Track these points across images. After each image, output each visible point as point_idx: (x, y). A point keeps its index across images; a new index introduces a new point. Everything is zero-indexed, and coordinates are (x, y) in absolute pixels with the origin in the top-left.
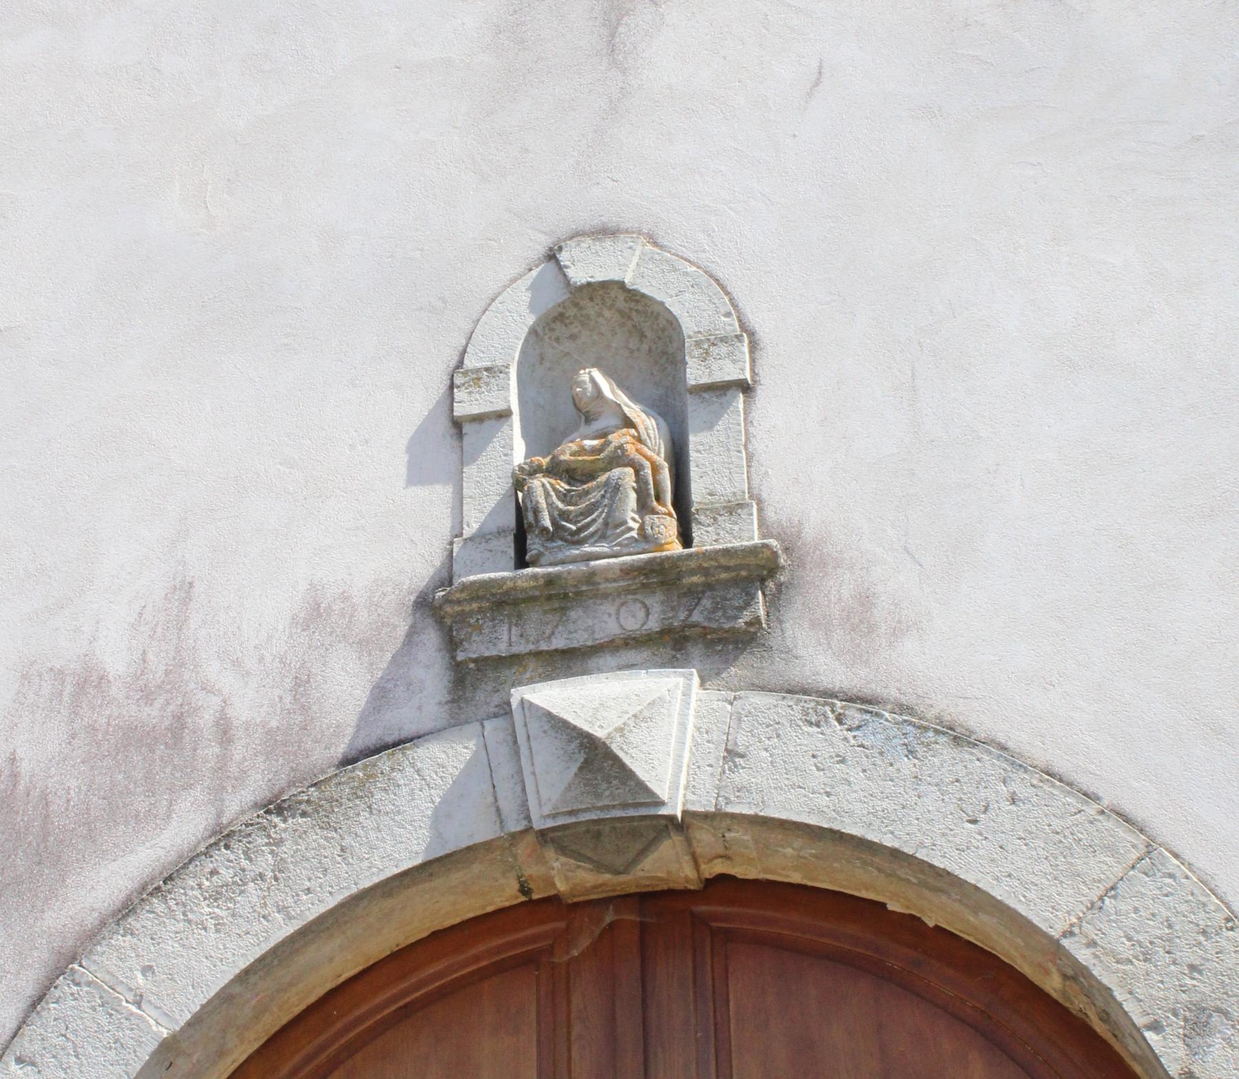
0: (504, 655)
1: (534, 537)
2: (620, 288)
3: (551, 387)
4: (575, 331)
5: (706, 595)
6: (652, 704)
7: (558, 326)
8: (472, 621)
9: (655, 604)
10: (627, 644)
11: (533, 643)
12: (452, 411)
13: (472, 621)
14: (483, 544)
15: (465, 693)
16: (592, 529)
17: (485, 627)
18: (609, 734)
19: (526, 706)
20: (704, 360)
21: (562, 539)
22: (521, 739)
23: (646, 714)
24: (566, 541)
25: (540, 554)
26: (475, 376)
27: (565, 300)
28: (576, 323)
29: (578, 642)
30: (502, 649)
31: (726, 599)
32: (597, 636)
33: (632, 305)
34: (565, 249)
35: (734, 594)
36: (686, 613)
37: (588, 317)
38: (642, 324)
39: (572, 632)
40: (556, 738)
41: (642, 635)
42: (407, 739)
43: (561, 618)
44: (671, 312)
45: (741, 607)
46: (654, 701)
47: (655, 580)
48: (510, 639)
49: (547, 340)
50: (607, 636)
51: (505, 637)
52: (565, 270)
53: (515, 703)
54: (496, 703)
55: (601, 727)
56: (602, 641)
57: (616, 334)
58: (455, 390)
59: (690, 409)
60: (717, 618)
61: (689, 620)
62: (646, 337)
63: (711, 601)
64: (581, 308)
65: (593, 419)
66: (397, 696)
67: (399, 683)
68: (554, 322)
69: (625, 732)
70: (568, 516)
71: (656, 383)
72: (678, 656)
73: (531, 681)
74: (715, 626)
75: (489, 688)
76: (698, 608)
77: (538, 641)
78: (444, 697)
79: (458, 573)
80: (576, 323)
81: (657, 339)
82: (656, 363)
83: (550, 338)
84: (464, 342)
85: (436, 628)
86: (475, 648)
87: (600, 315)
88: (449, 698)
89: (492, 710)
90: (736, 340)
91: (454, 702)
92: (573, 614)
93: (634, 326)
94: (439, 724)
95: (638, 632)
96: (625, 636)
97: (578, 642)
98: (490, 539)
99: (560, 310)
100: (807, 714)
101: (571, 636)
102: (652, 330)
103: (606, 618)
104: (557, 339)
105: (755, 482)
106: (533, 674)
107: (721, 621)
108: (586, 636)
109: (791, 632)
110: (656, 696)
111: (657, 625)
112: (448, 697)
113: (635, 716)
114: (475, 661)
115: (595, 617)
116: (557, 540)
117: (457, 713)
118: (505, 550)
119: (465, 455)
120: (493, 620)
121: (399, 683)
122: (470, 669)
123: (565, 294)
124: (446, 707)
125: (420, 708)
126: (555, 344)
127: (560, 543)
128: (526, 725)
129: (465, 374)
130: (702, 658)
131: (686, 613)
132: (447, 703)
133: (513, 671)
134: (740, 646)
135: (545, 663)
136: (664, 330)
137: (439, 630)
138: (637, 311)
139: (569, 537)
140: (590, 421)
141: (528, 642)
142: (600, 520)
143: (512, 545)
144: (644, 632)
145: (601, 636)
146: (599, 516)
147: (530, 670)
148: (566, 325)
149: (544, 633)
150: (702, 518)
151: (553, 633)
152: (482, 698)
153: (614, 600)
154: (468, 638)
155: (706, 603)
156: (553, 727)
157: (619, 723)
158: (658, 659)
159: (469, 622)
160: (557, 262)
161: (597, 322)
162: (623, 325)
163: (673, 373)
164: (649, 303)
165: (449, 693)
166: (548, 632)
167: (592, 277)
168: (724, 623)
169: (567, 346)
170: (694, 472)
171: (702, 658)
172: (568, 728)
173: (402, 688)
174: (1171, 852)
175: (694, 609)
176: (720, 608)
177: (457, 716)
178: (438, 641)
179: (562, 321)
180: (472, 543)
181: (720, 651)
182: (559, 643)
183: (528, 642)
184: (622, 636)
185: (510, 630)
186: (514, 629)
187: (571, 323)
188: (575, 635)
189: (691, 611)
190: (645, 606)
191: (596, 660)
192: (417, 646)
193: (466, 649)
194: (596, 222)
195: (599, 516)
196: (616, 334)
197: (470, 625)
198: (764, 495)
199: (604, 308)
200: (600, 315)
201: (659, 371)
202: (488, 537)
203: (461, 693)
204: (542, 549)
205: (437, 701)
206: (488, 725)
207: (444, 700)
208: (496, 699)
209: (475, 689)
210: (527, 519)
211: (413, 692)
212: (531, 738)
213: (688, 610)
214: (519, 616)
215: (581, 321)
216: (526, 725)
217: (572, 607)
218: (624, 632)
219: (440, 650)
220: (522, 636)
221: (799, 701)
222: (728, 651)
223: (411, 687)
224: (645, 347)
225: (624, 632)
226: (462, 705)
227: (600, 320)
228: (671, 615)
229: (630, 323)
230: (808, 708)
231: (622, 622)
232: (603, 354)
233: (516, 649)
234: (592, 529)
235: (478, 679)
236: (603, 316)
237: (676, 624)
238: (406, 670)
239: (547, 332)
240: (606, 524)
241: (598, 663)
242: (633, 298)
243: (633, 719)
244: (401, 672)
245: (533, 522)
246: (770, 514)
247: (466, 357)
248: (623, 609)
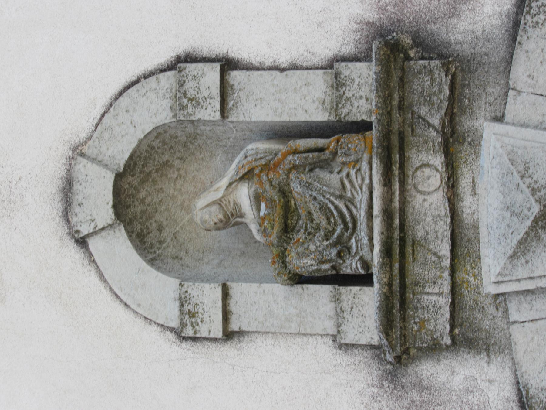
0: (450, 300)
1: (344, 265)
2: (121, 178)
3: (203, 253)
4: (154, 225)
5: (417, 110)
6: (512, 163)
7: (148, 240)
8: (415, 328)
9: (419, 159)
10: (453, 186)
11: (443, 272)
12: (215, 340)
13: (415, 328)
14: (345, 314)
15: (482, 339)
16: (345, 210)
17: (423, 316)
18: (536, 201)
19: (500, 279)
20: (198, 103)
21: (350, 239)
22: (530, 285)
23: (521, 168)
24: (352, 234)
25: (362, 259)
26: (187, 316)
27: (126, 230)
28: (148, 224)
29: (446, 230)
30: (444, 302)
31: (422, 92)
32: (443, 213)
33: (138, 170)
34: (79, 228)
35: (419, 84)
36: (431, 129)
37: (143, 212)
38: (156, 163)
39: (437, 236)
40: (534, 252)
41: (447, 171)
42: (518, 394)
43: (422, 246)
44: (150, 132)
45: (431, 78)
46: (510, 160)
47: (398, 156)
48: (436, 294)
49: (160, 251)
50: (444, 204)
51: (434, 298)
52: (97, 229)
53: (494, 290)
54: (495, 309)
55: (529, 209)
56: (448, 208)
57: (161, 189)
58: (198, 335)
59: (241, 118)
60: (439, 101)
61: (437, 127)
62: (168, 161)
63: (422, 107)
64: (135, 217)
65: (240, 211)
66: (476, 403)
67: (465, 400)
68: (144, 243)
69: (536, 187)
70: (329, 231)
71: (210, 156)
72: (469, 140)
73: (478, 276)
74: (446, 104)
75: (480, 316)
76: (427, 119)
77: (441, 268)
78: (483, 358)
79: (369, 340)
80: (148, 224)
81: (172, 151)
82: (193, 154)
83: (159, 249)
84: (154, 327)
85: (418, 363)
86: (441, 327)
87: (143, 201)
88: (485, 353)
89: (500, 313)
90: (183, 73)
91: (489, 350)
92: (420, 234)
93: (157, 171)
94: (508, 363)
95: (444, 175)
96: (446, 187)
97: (446, 230)
98: (341, 309)
99: (134, 236)
100: (537, 23)
101: (440, 237)
102: (163, 154)
103: (426, 204)
104: (161, 242)
105: (317, 61)
106: (471, 274)
107: (442, 98)
108: (442, 223)
109: (459, 35)
110: (506, 158)
111: (439, 157)
112: (484, 355)
113: (522, 177)
114: (453, 327)
115: (425, 214)
116: (350, 244)
117: (500, 347)
118: (353, 296)
119: (259, 330)
120: (417, 308)
121: (465, 400)
122: (459, 332)
123: (120, 230)
124: (492, 356)
125: (491, 382)
126: (165, 245)
127: (353, 240)
128: (519, 280)
129: (183, 325)
130: (475, 118)
131: (431, 129)
132: (488, 356)
133: (466, 293)
134: (467, 82)
135: (462, 263)
136: (164, 143)
137: (420, 360)
138: (143, 166)
139: (349, 232)
140: (242, 213)
141: (441, 277)
142: (337, 202)
143: (349, 288)
144: (444, 169)
145: (444, 210)
146: (333, 203)
147: (467, 277)
148: (149, 233)
149: (434, 262)
150: (345, 111)
151: (435, 254)
152: (488, 322)
153: (411, 196)
154: (431, 333)
155: (423, 111)
156: (524, 254)
157: (528, 191)
158: (471, 158)
159: (416, 331)
160: (89, 235)
161: (149, 205)
162: (154, 182)
163: (204, 138)
164: (138, 153)
165: (480, 353)
166: (434, 258)
167: (108, 204)
168: (444, 95)
169: (167, 234)
170: (301, 117)
171: (475, 118)
172: (526, 240)
173: (471, 397)
174: (502, 282)
175: (428, 122)
176: (430, 98)
177: (502, 347)
178: (430, 362)
179: (144, 236)
180: (343, 325)
181: (469, 101)
182: (445, 249)
183: (441, 277)
184: (445, 190)
185: (428, 294)
186: (427, 290)
187: (147, 228)
188: (439, 234)
189: (430, 125)
190: (420, 167)
191: (465, 216)
192: (432, 382)
193: (441, 335)
194: (58, 197)
195: (333, 203)
196: (161, 189)
197: (419, 330)
198: (330, 54)
199: (138, 196)
200: (143, 201)
201: (201, 153)
202: (339, 310)
203: (481, 342)
204: (357, 258)
205: (485, 365)
206: (514, 316)
207: (486, 358)
208: (491, 310)
209: (479, 329)
210: (326, 271)
211: (475, 387)
212: (532, 275)
213: (429, 128)
214: (417, 284)
215: (147, 220)
216: (519, 280)
217: (413, 234)
218: (441, 188)
219: (439, 360)
220: (434, 283)
221: (525, 30)
222: (470, 94)
223: (471, 389)
224: (177, 162)
225: (441, 188)
226: (493, 342)
227: (147, 201)
228: (431, 143)
229: (154, 175)
230: (532, 22)
231: (432, 189)
232: (179, 203)
233: (446, 288)
234: (345, 210)
235: (470, 326)
236: (145, 198)
237: (440, 140)
238: (454, 393)
239: (153, 250)
240: (341, 197)
241: (468, 215)
242: (131, 168)
243: (525, 179)
244: (455, 398)
245: (331, 264)
246: (347, 50)
247: (167, 325)
248: (420, 188)
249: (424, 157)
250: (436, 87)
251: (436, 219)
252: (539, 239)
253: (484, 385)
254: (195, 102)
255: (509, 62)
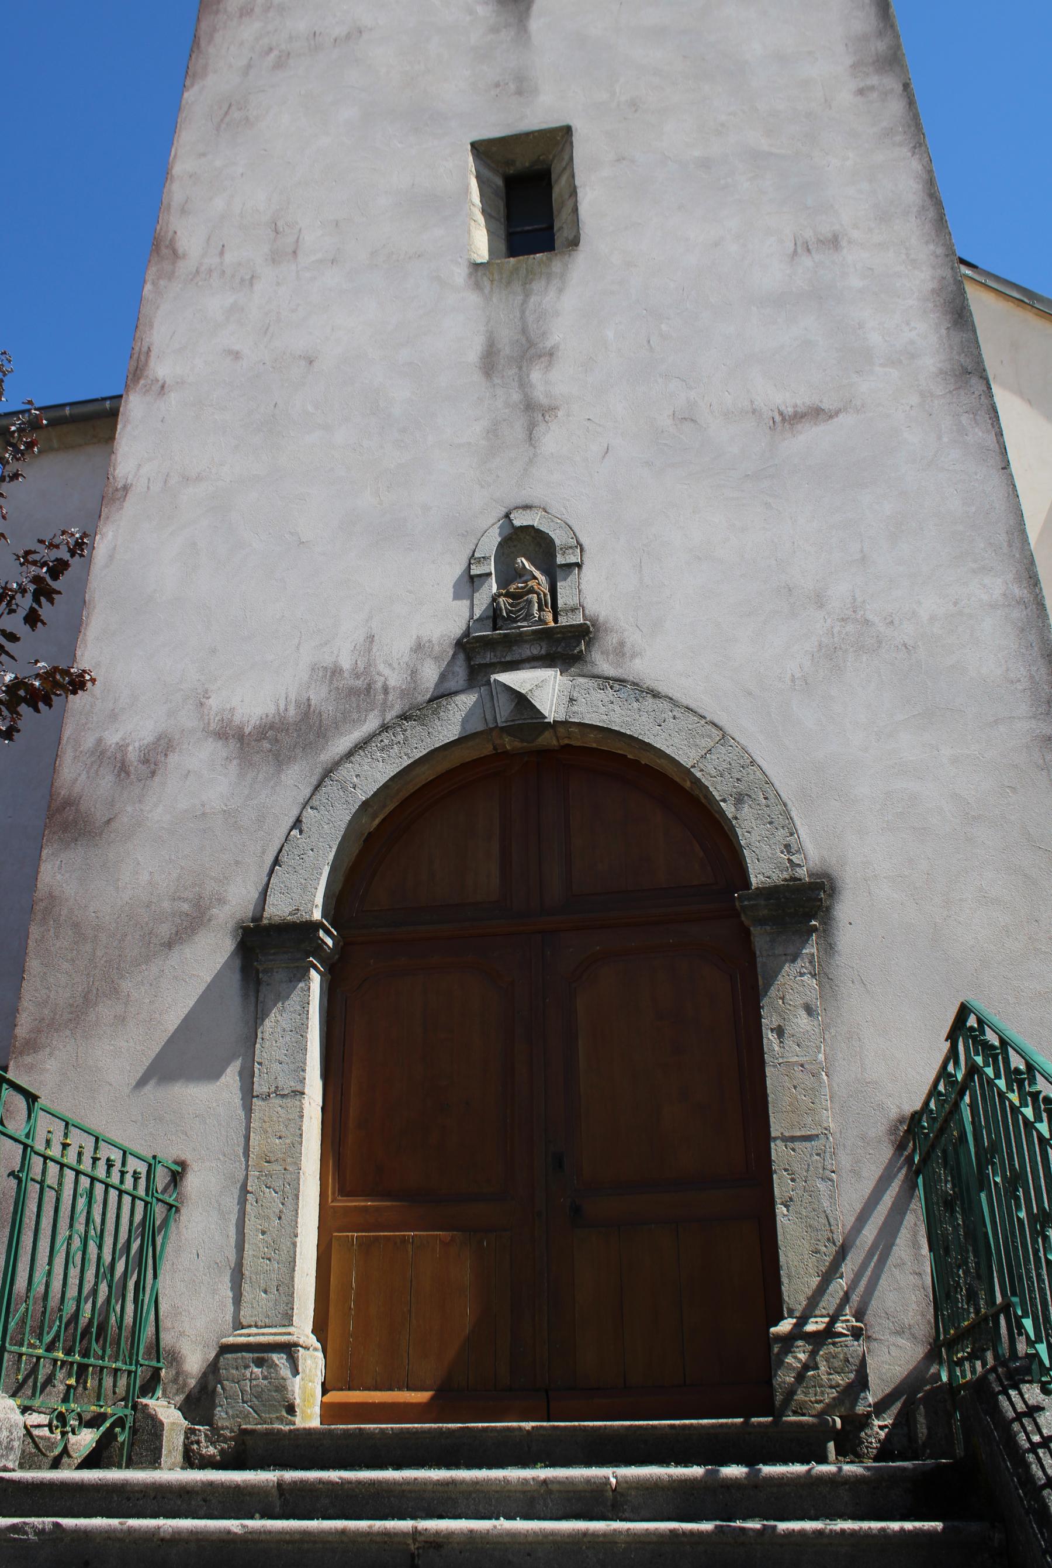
6: (543, 681)
30: (488, 660)
51: (489, 656)
105: (582, 600)
129: (475, 559)
145: (524, 656)
157: (531, 688)
182: (508, 659)
194: (524, 504)
200: (525, 538)
224: (541, 550)
246: (587, 612)
249: (544, 646)
250: (640, 642)
251: (520, 654)
252: (512, 695)
253: (456, 679)
254: (564, 554)
255: (583, 676)
